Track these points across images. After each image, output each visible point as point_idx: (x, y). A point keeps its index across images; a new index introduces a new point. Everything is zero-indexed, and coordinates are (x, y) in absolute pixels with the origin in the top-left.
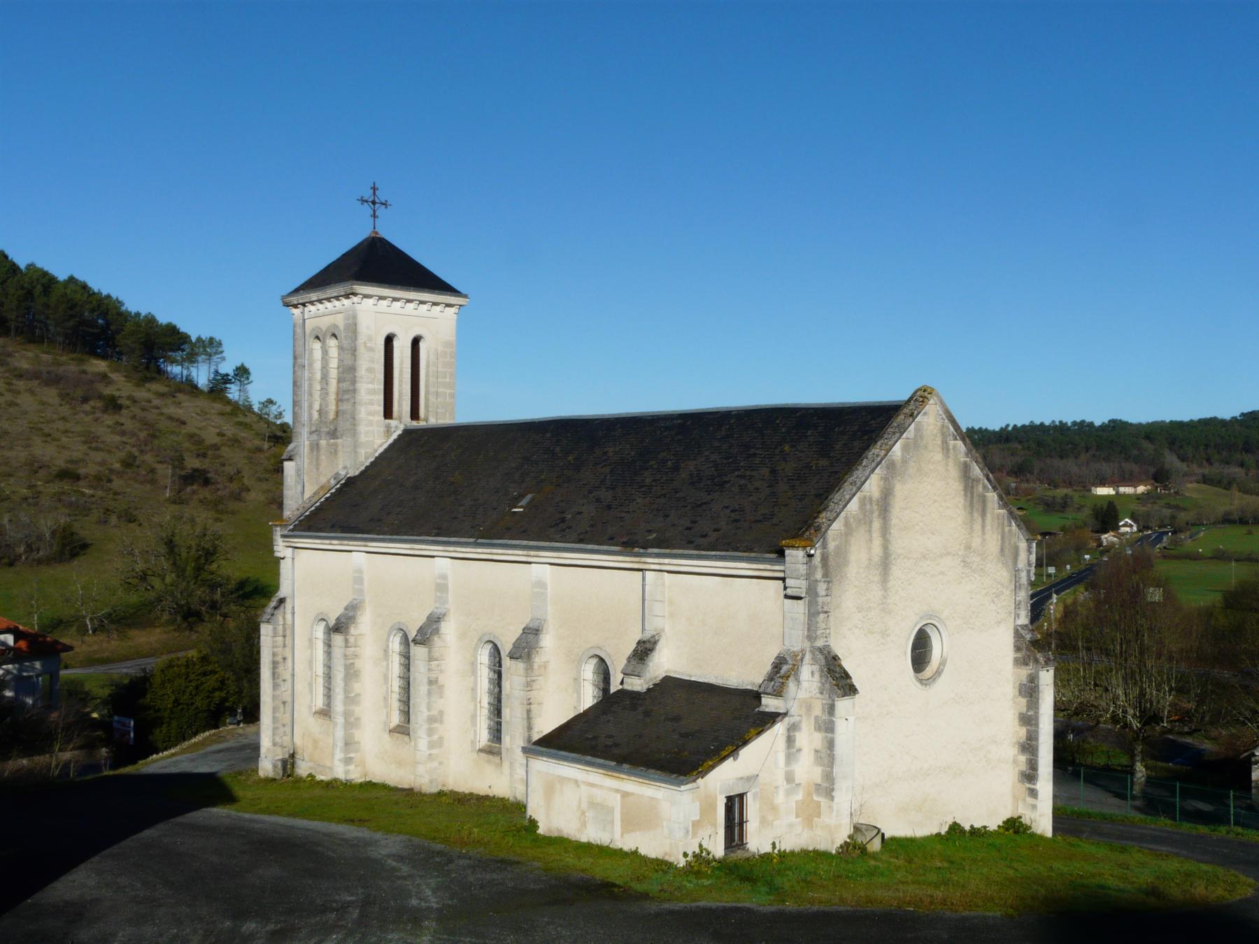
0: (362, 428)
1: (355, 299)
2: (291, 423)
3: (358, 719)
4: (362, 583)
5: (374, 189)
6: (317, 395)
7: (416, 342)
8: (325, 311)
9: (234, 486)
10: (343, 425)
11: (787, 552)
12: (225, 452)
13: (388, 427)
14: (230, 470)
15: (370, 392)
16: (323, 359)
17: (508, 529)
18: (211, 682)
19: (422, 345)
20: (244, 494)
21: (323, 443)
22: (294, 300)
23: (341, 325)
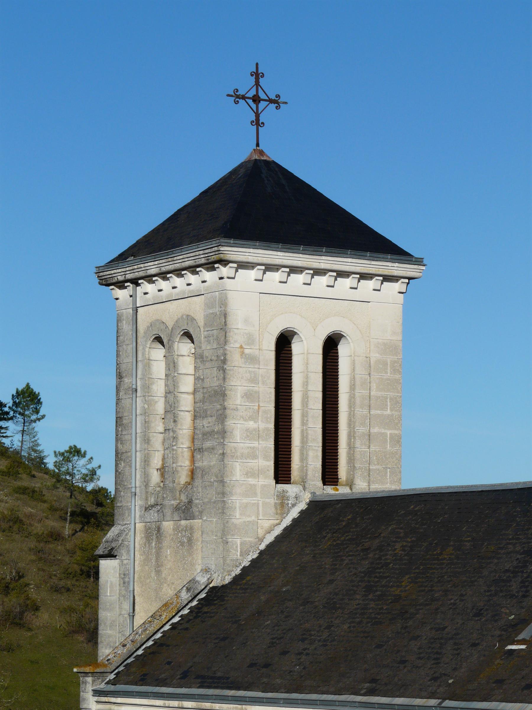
0: (237, 500)
1: (224, 271)
2: (111, 489)
5: (257, 75)
6: (157, 441)
7: (331, 344)
8: (172, 295)
10: (203, 494)
13: (282, 497)
15: (254, 435)
16: (168, 376)
17: (500, 682)
19: (343, 350)
20: (28, 616)
21: (168, 526)
22: (118, 274)
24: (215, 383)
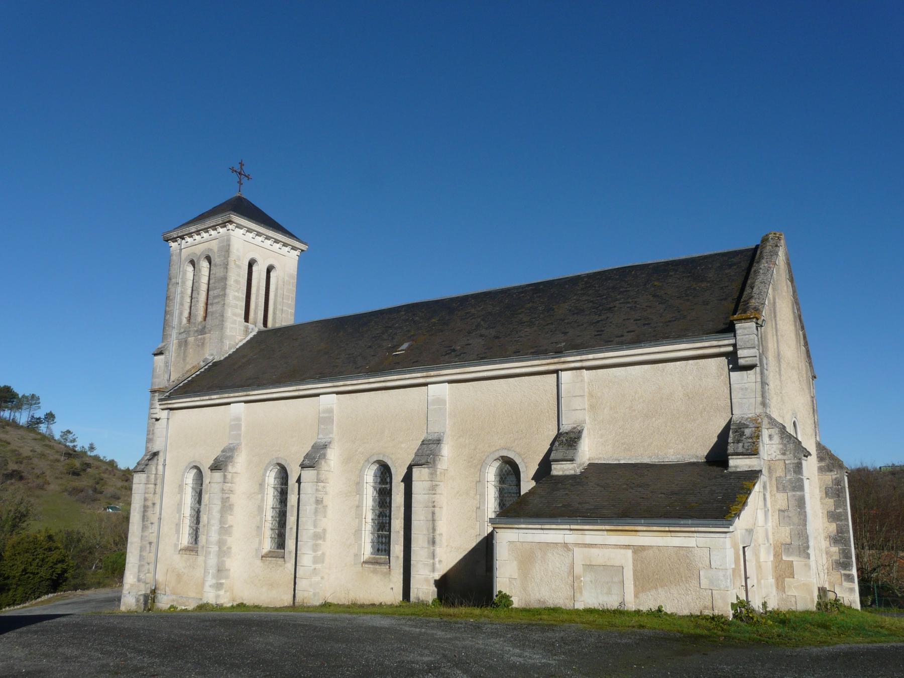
0: (228, 325)
1: (230, 227)
3: (230, 548)
4: (240, 430)
6: (187, 306)
7: (269, 270)
9: (40, 481)
11: (738, 326)
12: (35, 461)
14: (38, 472)
15: (237, 298)
18: (55, 555)
20: (46, 486)
21: (191, 339)
23: (216, 249)
24: (222, 274)
